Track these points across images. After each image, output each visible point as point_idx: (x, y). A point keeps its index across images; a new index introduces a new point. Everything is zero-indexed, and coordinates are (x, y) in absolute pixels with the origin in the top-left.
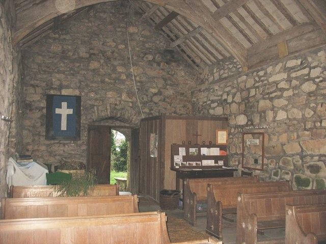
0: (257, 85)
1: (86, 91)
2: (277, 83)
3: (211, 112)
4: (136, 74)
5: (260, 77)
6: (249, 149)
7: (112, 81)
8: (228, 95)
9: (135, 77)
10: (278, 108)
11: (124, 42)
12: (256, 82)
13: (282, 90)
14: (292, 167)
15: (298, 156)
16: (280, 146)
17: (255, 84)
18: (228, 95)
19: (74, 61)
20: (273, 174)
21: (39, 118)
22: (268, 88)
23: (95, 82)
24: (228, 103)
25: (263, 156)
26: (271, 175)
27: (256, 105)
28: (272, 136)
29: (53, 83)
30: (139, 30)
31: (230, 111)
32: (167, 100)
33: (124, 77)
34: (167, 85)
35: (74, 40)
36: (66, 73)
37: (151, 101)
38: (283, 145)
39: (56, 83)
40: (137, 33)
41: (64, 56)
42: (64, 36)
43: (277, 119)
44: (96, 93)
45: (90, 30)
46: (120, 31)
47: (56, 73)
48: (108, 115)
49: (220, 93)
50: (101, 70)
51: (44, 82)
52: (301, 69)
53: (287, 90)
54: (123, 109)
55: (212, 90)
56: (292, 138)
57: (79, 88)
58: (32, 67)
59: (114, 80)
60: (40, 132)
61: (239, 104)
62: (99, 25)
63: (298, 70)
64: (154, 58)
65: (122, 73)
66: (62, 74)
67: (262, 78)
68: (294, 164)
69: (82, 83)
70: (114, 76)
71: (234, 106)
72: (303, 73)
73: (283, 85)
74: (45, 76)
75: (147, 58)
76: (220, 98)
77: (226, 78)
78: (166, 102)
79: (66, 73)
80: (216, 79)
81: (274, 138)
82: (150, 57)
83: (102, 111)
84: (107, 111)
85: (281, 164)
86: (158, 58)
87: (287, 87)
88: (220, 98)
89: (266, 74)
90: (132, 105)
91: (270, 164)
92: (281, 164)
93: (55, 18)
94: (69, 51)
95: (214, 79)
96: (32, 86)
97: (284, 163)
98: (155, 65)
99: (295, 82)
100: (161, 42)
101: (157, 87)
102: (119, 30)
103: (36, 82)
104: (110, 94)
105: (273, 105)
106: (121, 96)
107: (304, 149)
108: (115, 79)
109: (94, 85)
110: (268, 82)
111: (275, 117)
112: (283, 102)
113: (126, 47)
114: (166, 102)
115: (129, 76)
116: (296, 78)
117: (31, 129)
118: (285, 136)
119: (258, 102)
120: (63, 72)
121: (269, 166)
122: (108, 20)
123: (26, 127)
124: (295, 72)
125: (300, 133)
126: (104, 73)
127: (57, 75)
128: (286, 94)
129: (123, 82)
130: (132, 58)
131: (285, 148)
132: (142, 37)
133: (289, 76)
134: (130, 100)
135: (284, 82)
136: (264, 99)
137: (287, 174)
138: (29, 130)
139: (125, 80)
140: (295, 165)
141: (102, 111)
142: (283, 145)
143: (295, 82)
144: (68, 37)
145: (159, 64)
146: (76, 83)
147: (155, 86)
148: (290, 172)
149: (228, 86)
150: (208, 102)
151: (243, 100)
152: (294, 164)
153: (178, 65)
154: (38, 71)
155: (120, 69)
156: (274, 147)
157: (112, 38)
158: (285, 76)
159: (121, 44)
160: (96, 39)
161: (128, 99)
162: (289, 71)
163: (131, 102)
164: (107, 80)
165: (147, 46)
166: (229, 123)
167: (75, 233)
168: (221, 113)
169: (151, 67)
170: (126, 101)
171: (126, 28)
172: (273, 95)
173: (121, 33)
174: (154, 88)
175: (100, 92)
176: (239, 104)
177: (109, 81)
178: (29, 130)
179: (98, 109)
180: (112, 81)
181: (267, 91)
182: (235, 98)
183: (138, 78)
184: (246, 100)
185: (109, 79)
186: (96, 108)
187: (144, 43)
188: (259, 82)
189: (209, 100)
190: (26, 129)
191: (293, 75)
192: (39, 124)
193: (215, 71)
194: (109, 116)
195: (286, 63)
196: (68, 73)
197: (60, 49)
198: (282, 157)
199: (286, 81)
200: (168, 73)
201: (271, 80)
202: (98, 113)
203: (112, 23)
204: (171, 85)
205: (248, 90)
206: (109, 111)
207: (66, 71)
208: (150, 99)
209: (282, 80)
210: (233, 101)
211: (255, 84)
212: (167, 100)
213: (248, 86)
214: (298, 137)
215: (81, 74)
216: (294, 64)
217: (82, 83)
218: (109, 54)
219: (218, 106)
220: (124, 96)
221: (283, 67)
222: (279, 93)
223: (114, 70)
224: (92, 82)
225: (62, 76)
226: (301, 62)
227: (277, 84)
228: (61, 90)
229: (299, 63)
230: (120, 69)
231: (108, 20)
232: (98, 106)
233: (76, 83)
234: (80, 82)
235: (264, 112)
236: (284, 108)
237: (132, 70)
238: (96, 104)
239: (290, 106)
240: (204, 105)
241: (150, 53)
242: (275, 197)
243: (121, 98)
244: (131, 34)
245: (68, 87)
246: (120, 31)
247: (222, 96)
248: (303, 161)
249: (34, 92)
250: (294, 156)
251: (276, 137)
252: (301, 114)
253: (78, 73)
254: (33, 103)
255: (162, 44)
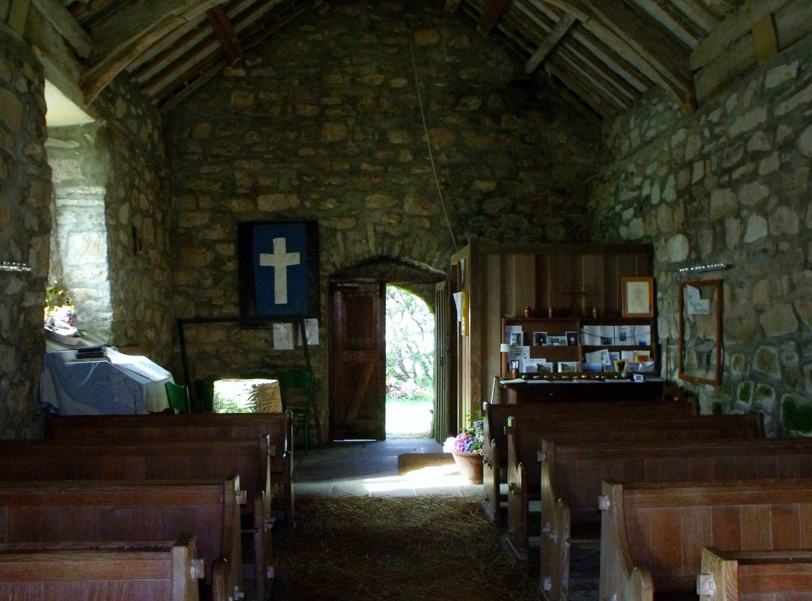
0: (707, 149)
2: (744, 138)
4: (437, 148)
5: (711, 126)
6: (694, 326)
7: (377, 168)
8: (652, 184)
9: (435, 153)
10: (748, 208)
13: (756, 156)
14: (778, 376)
15: (792, 343)
17: (702, 147)
18: (652, 184)
20: (738, 392)
22: (729, 157)
24: (653, 206)
25: (720, 344)
26: (735, 396)
27: (706, 206)
28: (738, 290)
30: (441, 36)
31: (658, 228)
33: (406, 156)
37: (480, 212)
38: (759, 311)
39: (242, 181)
42: (260, 71)
43: (749, 239)
45: (319, 50)
46: (394, 46)
48: (368, 252)
50: (350, 143)
51: (216, 181)
53: (768, 154)
54: (406, 235)
55: (623, 176)
57: (298, 190)
59: (382, 165)
60: (211, 299)
61: (672, 205)
63: (791, 95)
64: (484, 106)
65: (403, 146)
68: (781, 364)
70: (380, 155)
71: (664, 211)
72: (801, 101)
73: (757, 143)
74: (218, 169)
75: (465, 105)
76: (636, 194)
77: (652, 139)
79: (266, 156)
80: (635, 145)
82: (474, 103)
83: (354, 242)
84: (367, 241)
85: (756, 367)
87: (767, 147)
88: (636, 194)
89: (724, 115)
90: (432, 224)
91: (735, 368)
92: (756, 367)
93: (694, 83)
95: (630, 146)
96: (191, 192)
97: (763, 363)
98: (487, 122)
99: (784, 131)
102: (390, 42)
103: (198, 182)
104: (374, 201)
105: (739, 203)
110: (728, 138)
111: (742, 236)
112: (757, 191)
113: (412, 83)
115: (419, 152)
116: (787, 118)
117: (191, 291)
119: (708, 196)
121: (732, 370)
123: (181, 288)
124: (785, 99)
125: (796, 276)
126: (357, 150)
127: (246, 164)
128: (767, 166)
129: (406, 168)
133: (770, 112)
134: (425, 213)
135: (760, 134)
136: (721, 186)
137: (767, 393)
138: (187, 295)
140: (783, 368)
141: (354, 242)
142: (759, 311)
143: (784, 131)
144: (268, 72)
145: (496, 117)
146: (290, 180)
147: (486, 172)
148: (773, 389)
149: (127, 127)
154: (201, 158)
155: (396, 138)
156: (741, 320)
158: (760, 115)
159: (399, 76)
163: (426, 217)
164: (365, 166)
165: (464, 76)
168: (641, 233)
170: (415, 216)
173: (395, 50)
174: (486, 179)
176: (672, 205)
177: (371, 169)
178: (187, 295)
179: (345, 238)
180: (377, 168)
181: (726, 165)
183: (443, 158)
184: (686, 194)
185: (372, 164)
186: (339, 236)
188: (710, 141)
189: (620, 202)
191: (781, 110)
192: (208, 282)
194: (373, 253)
195: (764, 78)
196: (270, 156)
198: (758, 346)
199: (764, 131)
202: (346, 248)
205: (690, 165)
206: (372, 241)
208: (475, 208)
209: (756, 129)
210: (662, 201)
211: (702, 147)
214: (792, 287)
215: (302, 157)
216: (784, 78)
218: (369, 101)
219: (635, 216)
220: (409, 205)
222: (748, 168)
223: (383, 142)
225: (256, 165)
226: (799, 69)
227: (746, 141)
229: (794, 73)
230: (396, 138)
232: (344, 232)
233: (290, 180)
234: (300, 175)
235: (721, 222)
236: (762, 209)
237: (426, 138)
238: (340, 226)
239: (773, 202)
240: (610, 214)
244: (424, 49)
245: (269, 190)
247: (640, 188)
248: (801, 356)
252: (796, 223)
255: (501, 68)
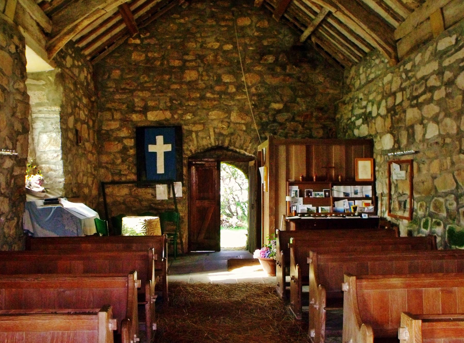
1: (180, 112)
2: (425, 79)
3: (356, 132)
4: (250, 84)
5: (407, 72)
8: (373, 105)
9: (249, 87)
10: (427, 119)
11: (231, 40)
12: (403, 81)
13: (432, 89)
14: (444, 214)
15: (453, 196)
16: (430, 178)
17: (401, 84)
18: (373, 105)
19: (163, 72)
21: (118, 152)
22: (416, 89)
23: (193, 99)
25: (412, 196)
27: (403, 117)
29: (136, 105)
30: (252, 21)
32: (297, 119)
33: (232, 89)
34: (297, 96)
35: (162, 44)
36: (152, 89)
37: (275, 121)
40: (250, 26)
41: (149, 67)
44: (194, 114)
46: (225, 26)
47: (139, 90)
48: (211, 144)
49: (364, 103)
51: (124, 103)
52: (457, 51)
53: (438, 88)
54: (232, 134)
55: (356, 100)
56: (445, 167)
58: (109, 86)
59: (218, 94)
60: (120, 170)
62: (195, 20)
63: (452, 54)
64: (277, 60)
65: (230, 83)
66: (147, 92)
67: (410, 74)
68: (446, 208)
69: (174, 102)
72: (458, 58)
73: (433, 82)
74: (125, 96)
76: (363, 111)
77: (373, 80)
78: (297, 121)
79: (152, 89)
80: (363, 83)
81: (424, 168)
83: (202, 138)
84: (210, 138)
85: (432, 210)
86: (283, 58)
87: (438, 84)
89: (414, 66)
90: (247, 127)
92: (432, 210)
94: (155, 59)
95: (360, 83)
96: (109, 109)
98: (278, 70)
99: (448, 75)
100: (285, 36)
101: (282, 100)
102: (223, 24)
104: (214, 115)
106: (229, 117)
107: (460, 184)
108: (220, 93)
109: (191, 103)
110: (416, 79)
111: (424, 135)
112: (432, 110)
114: (297, 121)
115: (240, 87)
116: (450, 67)
117: (109, 166)
118: (435, 165)
119: (405, 112)
120: (148, 89)
122: (208, 11)
123: (104, 165)
124: (449, 56)
125: (455, 158)
127: (140, 94)
129: (232, 96)
130: (244, 62)
131: (436, 182)
132: (257, 31)
134: (243, 122)
136: (412, 106)
137: (438, 224)
138: (107, 168)
139: (234, 94)
141: (202, 138)
143: (448, 75)
145: (283, 67)
146: (165, 103)
147: (278, 98)
148: (442, 222)
150: (353, 119)
151: (389, 110)
152: (446, 208)
153: (314, 67)
154: (115, 90)
155: (226, 79)
156: (423, 182)
157: (214, 37)
158: (434, 66)
159: (228, 43)
160: (192, 40)
161: (239, 120)
162: (441, 57)
163: (244, 124)
164: (208, 95)
166: (102, 146)
167: (7, 298)
169: (273, 72)
170: (237, 123)
171: (235, 21)
172: (421, 100)
173: (226, 29)
175: (199, 113)
177: (212, 96)
178: (107, 168)
180: (216, 96)
181: (415, 94)
182: (381, 110)
183: (253, 90)
186: (194, 135)
187: (260, 39)
188: (406, 81)
189: (354, 116)
190: (103, 167)
191: (446, 63)
193: (361, 71)
194: (213, 144)
196: (154, 89)
197: (143, 57)
199: (437, 75)
200: (298, 79)
201: (419, 75)
202: (198, 142)
203: (213, 16)
204: (303, 97)
205: (394, 94)
206: (212, 137)
207: (153, 87)
209: (432, 74)
210: (378, 114)
212: (297, 119)
213: (394, 89)
214: (453, 163)
216: (448, 45)
217: (174, 102)
218: (211, 57)
220: (234, 117)
221: (433, 52)
224: (187, 100)
225: (146, 94)
226: (457, 39)
227: (426, 80)
228: (146, 112)
229: (454, 42)
231: (208, 11)
232: (197, 132)
234: (171, 100)
235: (412, 127)
236: (435, 119)
237: (243, 79)
238: (194, 129)
240: (349, 122)
241: (270, 53)
242: (376, 260)
243: (229, 119)
244: (242, 28)
245: (154, 108)
246: (225, 26)
249: (111, 118)
250: (446, 196)
251: (426, 165)
252: (455, 127)
253: (169, 88)
254: (111, 133)
255: (286, 39)
